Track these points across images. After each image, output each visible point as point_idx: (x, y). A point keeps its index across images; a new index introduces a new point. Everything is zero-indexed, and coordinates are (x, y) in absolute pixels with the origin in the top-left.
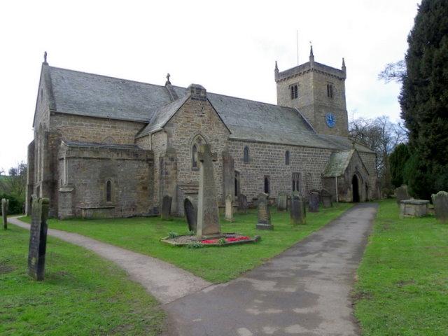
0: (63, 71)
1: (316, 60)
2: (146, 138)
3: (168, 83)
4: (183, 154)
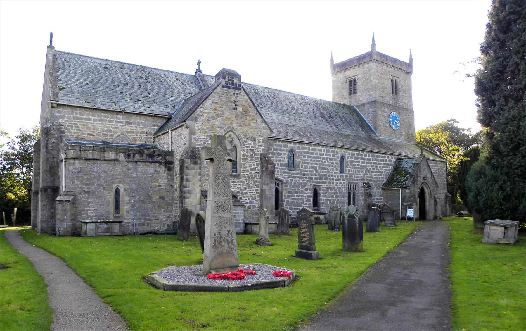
1: (379, 49)
3: (199, 71)
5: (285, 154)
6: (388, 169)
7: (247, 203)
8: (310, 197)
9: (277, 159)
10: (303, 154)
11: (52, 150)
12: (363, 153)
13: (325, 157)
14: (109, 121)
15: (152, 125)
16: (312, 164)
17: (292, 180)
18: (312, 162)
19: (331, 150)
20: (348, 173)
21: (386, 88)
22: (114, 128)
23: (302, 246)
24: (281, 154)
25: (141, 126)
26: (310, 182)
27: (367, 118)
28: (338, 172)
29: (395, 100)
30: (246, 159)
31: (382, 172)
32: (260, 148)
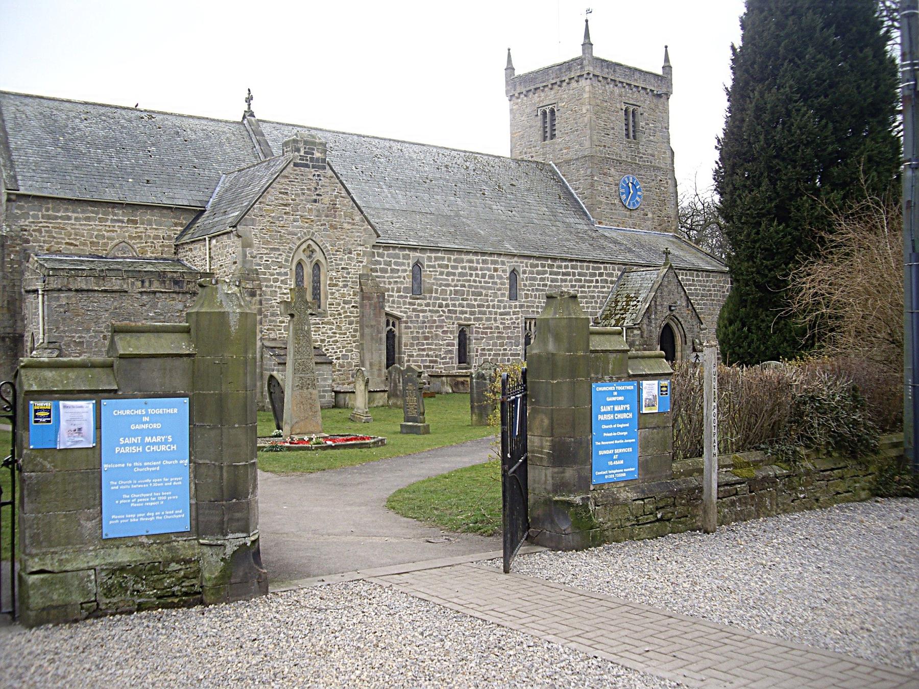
0: (27, 101)
1: (599, 52)
2: (197, 245)
4: (276, 281)
5: (405, 271)
6: (606, 290)
7: (338, 359)
8: (453, 345)
9: (391, 280)
10: (439, 270)
11: (11, 272)
12: (555, 262)
13: (480, 273)
14: (100, 220)
15: (171, 224)
16: (456, 286)
17: (418, 316)
18: (455, 282)
19: (491, 260)
20: (524, 300)
21: (613, 129)
22: (108, 231)
23: (408, 417)
24: (398, 270)
25: (154, 227)
26: (451, 318)
27: (576, 190)
28: (506, 299)
29: (632, 151)
30: (336, 285)
31: (593, 297)
32: (359, 266)
